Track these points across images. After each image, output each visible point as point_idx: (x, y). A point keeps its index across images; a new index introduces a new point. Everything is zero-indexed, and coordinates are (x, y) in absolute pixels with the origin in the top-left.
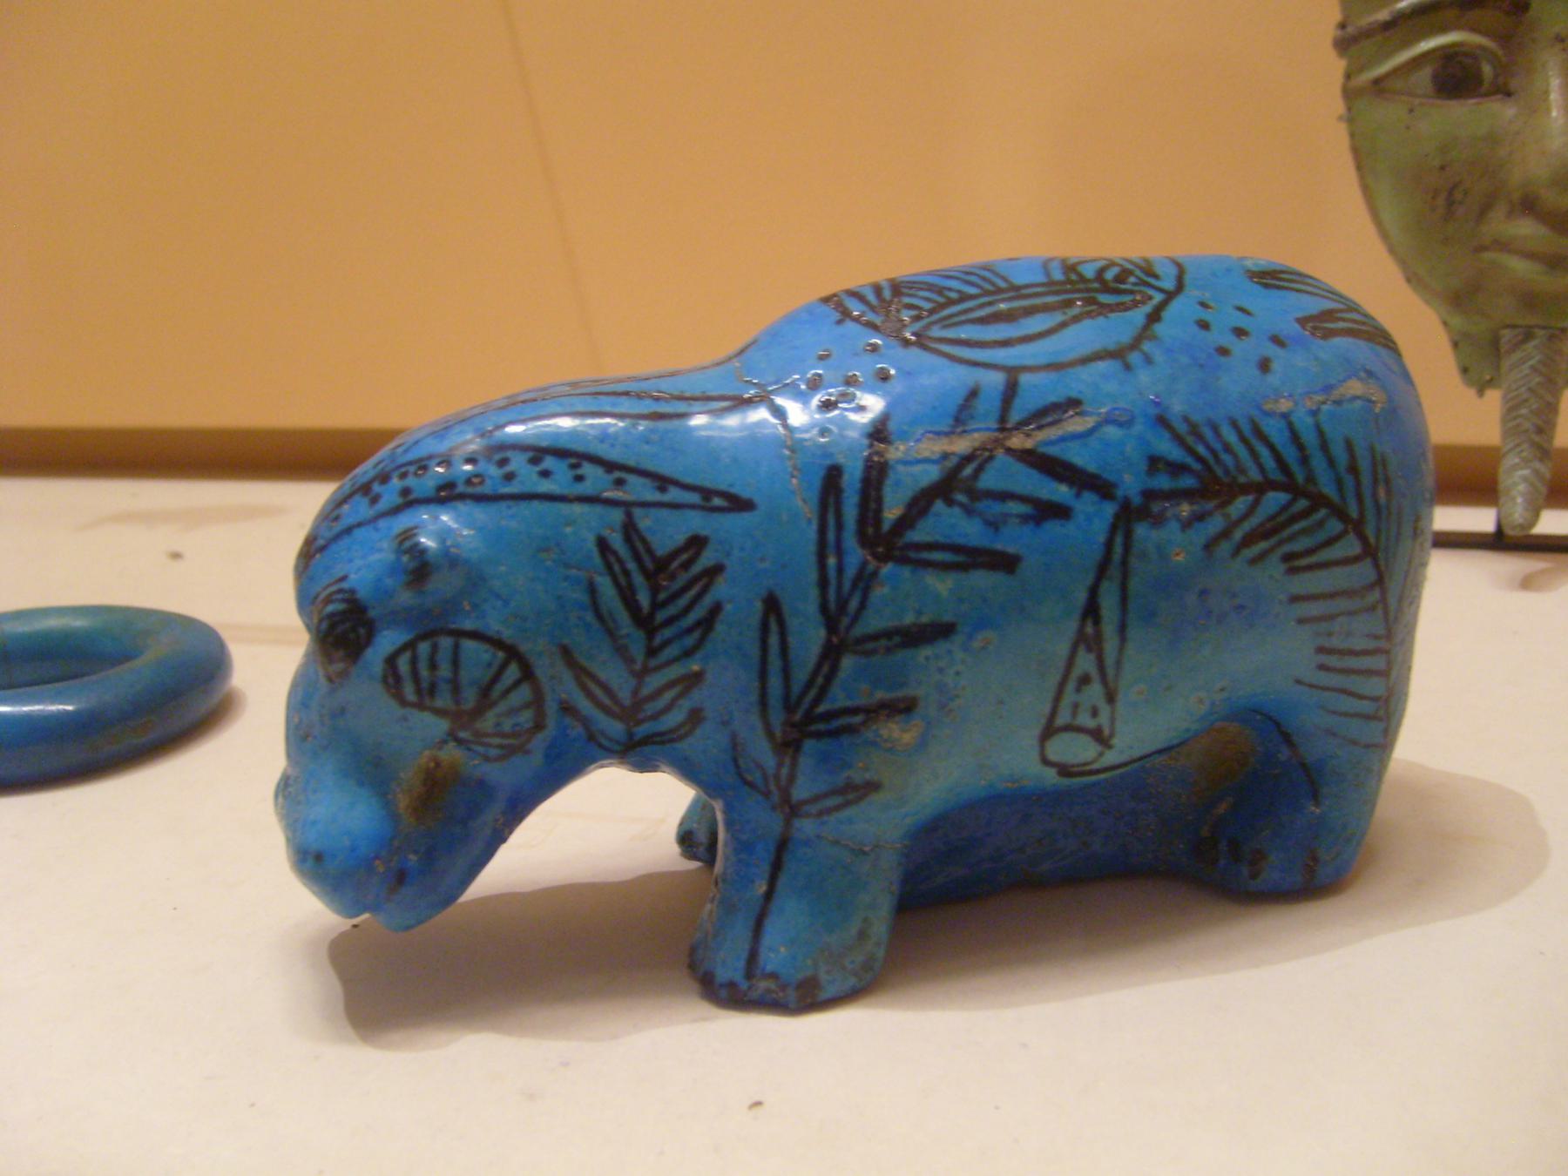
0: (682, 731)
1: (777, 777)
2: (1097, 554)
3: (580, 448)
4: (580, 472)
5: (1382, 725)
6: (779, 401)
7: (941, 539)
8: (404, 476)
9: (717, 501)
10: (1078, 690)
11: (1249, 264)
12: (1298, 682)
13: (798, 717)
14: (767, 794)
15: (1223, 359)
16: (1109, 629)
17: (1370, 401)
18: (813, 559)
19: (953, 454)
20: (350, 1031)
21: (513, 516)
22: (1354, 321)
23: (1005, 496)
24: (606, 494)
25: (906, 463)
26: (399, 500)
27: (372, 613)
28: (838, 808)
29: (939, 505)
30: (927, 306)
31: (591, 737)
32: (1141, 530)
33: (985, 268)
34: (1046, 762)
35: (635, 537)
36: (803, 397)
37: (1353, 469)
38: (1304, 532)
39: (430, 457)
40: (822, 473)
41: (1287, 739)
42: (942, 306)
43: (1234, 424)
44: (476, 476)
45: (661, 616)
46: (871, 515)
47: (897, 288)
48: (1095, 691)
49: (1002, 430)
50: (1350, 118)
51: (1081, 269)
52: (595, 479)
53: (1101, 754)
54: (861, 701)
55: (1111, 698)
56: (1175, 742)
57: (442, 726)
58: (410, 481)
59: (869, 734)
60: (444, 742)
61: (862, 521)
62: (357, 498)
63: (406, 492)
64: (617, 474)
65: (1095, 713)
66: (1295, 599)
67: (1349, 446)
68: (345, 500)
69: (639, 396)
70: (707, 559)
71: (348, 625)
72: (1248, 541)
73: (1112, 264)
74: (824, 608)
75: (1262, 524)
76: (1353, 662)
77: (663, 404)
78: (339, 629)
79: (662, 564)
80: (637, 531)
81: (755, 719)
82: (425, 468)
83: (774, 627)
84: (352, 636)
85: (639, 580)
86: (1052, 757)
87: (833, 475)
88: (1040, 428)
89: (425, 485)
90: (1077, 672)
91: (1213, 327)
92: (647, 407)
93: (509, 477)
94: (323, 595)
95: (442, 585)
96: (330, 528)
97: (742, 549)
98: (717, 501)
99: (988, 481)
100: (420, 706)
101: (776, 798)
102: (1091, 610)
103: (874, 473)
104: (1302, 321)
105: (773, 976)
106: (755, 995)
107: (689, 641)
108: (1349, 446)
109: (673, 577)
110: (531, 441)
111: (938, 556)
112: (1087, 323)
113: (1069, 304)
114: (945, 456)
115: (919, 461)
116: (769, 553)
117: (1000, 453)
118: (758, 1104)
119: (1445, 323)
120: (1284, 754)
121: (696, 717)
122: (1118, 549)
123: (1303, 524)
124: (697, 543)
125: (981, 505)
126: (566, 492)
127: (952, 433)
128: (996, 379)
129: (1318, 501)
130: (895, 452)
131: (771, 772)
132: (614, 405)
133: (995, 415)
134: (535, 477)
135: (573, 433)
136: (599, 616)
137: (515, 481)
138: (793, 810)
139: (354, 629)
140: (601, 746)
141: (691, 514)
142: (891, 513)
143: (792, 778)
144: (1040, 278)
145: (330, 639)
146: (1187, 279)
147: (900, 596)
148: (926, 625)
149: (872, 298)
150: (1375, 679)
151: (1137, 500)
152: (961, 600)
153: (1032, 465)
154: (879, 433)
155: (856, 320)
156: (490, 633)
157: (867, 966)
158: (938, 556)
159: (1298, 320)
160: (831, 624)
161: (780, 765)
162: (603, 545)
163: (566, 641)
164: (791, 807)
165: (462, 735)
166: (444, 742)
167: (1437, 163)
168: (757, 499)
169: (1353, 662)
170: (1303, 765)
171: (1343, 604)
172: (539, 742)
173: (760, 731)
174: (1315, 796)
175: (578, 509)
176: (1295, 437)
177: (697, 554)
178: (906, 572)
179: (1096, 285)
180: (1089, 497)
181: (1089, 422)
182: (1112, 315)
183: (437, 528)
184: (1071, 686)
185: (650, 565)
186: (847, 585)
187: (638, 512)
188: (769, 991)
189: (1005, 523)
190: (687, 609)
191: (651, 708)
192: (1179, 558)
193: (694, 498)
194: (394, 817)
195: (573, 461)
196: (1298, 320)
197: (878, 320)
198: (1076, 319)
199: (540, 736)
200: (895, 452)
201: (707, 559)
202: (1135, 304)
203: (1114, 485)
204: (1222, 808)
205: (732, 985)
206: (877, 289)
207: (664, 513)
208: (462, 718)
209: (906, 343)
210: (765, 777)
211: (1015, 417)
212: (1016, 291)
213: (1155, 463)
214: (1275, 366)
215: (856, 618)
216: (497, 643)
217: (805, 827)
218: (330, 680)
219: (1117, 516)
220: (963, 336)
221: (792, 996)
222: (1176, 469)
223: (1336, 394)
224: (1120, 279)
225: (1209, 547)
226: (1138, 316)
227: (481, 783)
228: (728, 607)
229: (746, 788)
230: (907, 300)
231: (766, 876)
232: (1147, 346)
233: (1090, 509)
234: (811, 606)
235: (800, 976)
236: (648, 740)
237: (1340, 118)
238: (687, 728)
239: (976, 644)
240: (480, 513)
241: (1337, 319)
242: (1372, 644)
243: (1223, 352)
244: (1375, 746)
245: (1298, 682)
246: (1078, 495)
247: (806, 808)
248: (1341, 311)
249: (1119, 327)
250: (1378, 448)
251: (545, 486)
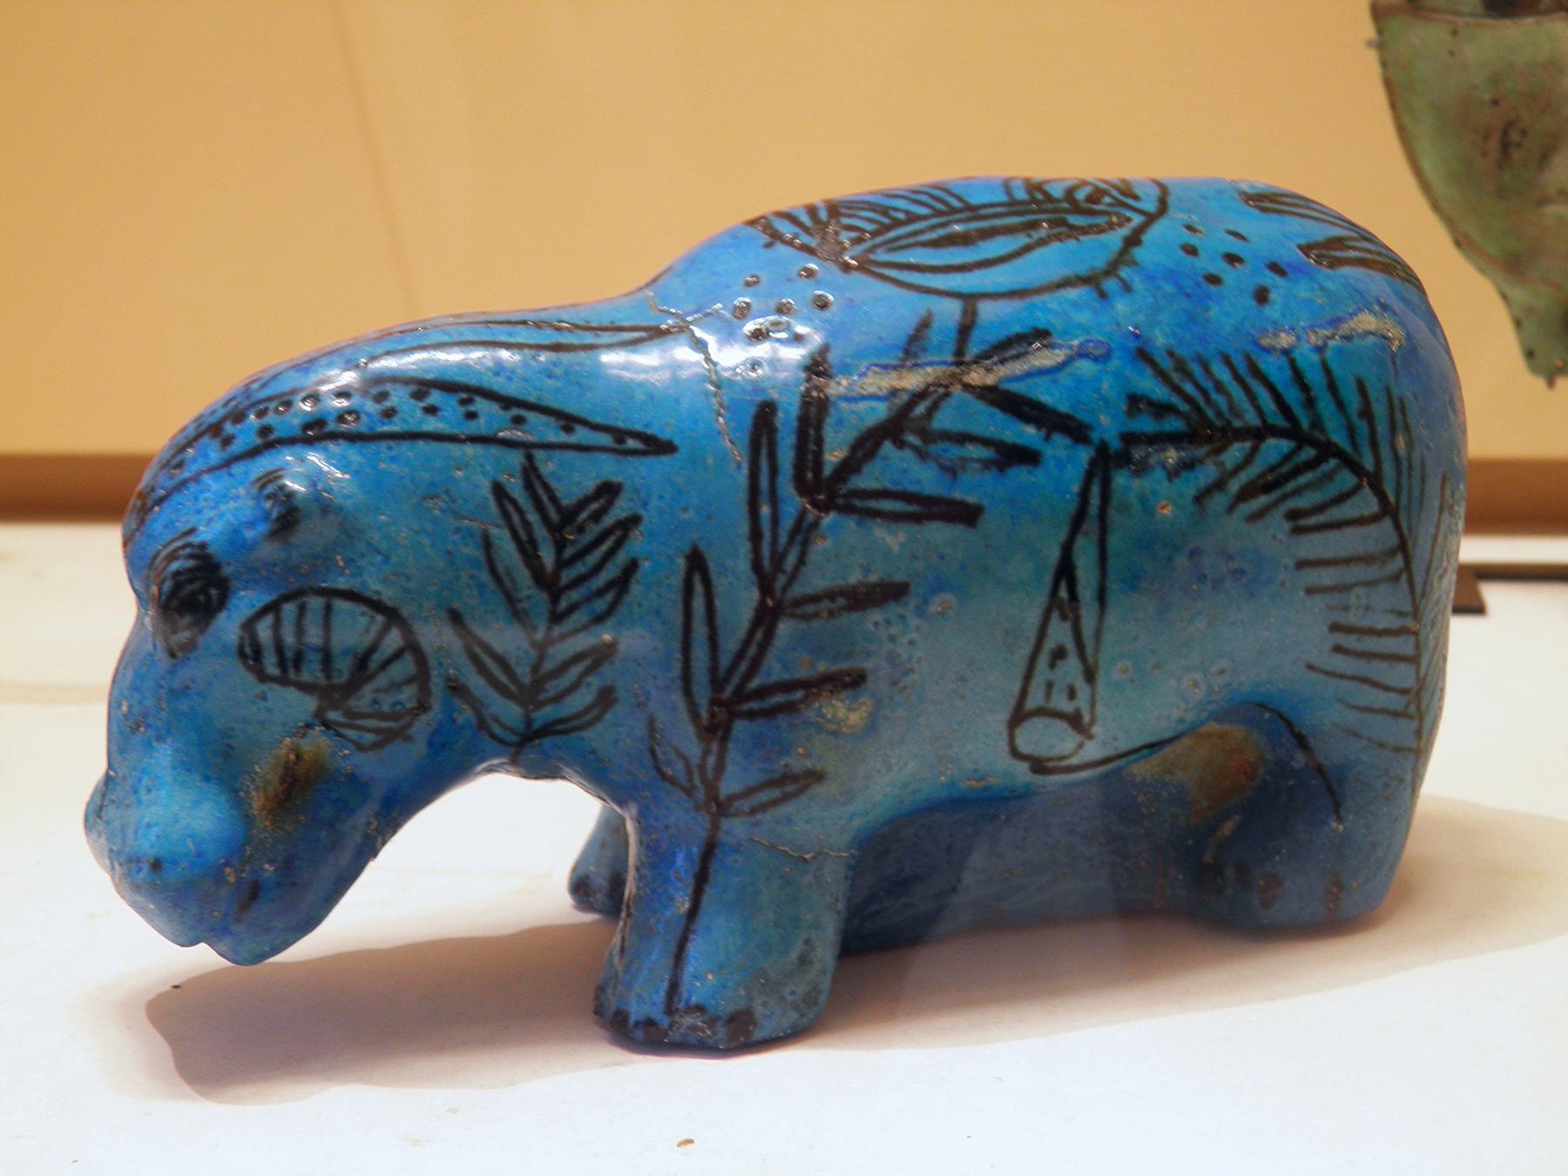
0: (588, 717)
1: (702, 768)
2: (1072, 507)
3: (473, 382)
4: (472, 408)
5: (1414, 725)
6: (698, 332)
7: (889, 485)
8: (261, 414)
9: (632, 443)
10: (1052, 666)
11: (1245, 187)
12: (1311, 667)
13: (727, 693)
14: (689, 792)
15: (1213, 289)
16: (1087, 592)
17: (1385, 337)
18: (744, 508)
19: (903, 390)
20: (186, 1088)
21: (393, 459)
22: (1369, 251)
23: (963, 438)
24: (501, 434)
25: (850, 399)
26: (259, 441)
27: (227, 571)
28: (774, 803)
29: (888, 447)
30: (870, 227)
31: (482, 724)
32: (1120, 479)
33: (936, 187)
34: (1015, 753)
35: (537, 485)
36: (728, 335)
37: (1367, 413)
38: (1308, 486)
39: (294, 392)
40: (753, 410)
41: (1301, 741)
42: (888, 228)
43: (1227, 361)
44: (350, 412)
45: (567, 576)
46: (810, 457)
47: (835, 209)
48: (1071, 668)
49: (959, 364)
50: (1381, 45)
51: (1047, 188)
52: (489, 416)
53: (1080, 746)
54: (802, 673)
55: (1090, 675)
56: (1167, 735)
57: (310, 703)
58: (270, 419)
59: (810, 713)
60: (309, 726)
61: (799, 467)
62: (206, 440)
63: (265, 431)
64: (516, 411)
65: (1072, 694)
66: (1302, 564)
67: (1362, 388)
68: (190, 443)
69: (538, 325)
70: (621, 509)
71: (196, 585)
72: (1246, 494)
73: (1084, 183)
74: (756, 566)
75: (1262, 475)
76: (1371, 644)
77: (568, 337)
78: (189, 588)
79: (569, 515)
80: (539, 477)
81: (677, 697)
82: (288, 404)
83: (698, 588)
84: (201, 598)
85: (541, 532)
86: (1023, 747)
87: (765, 413)
88: (1002, 361)
89: (287, 423)
90: (1049, 645)
91: (1201, 253)
92: (548, 337)
93: (389, 414)
94: (164, 554)
95: (310, 536)
96: (172, 477)
97: (661, 497)
98: (632, 443)
99: (944, 420)
100: (283, 681)
101: (701, 794)
102: (1065, 571)
103: (813, 410)
104: (1306, 249)
105: (700, 1009)
106: (675, 1035)
107: (601, 605)
108: (1362, 388)
109: (581, 530)
110: (419, 375)
111: (887, 505)
112: (1055, 246)
113: (1034, 225)
114: (894, 392)
115: (864, 398)
116: (694, 502)
117: (957, 390)
118: (690, 1141)
119: (1504, 297)
120: (1299, 760)
121: (606, 698)
122: (1095, 501)
123: (1308, 477)
124: (609, 491)
125: (934, 449)
126: (456, 431)
127: (903, 366)
128: (950, 311)
129: (1327, 450)
130: (837, 387)
131: (695, 761)
132: (510, 334)
133: (951, 346)
134: (419, 413)
135: (462, 366)
136: (493, 571)
137: (395, 419)
138: (721, 808)
139: (204, 590)
140: (493, 736)
141: (603, 457)
142: (833, 456)
143: (720, 767)
144: (1001, 197)
145: (175, 603)
146: (1171, 200)
147: (844, 551)
148: (876, 585)
149: (805, 219)
150: (1403, 666)
151: (1115, 444)
152: (915, 557)
153: (993, 403)
154: (816, 367)
155: (790, 243)
156: (367, 594)
157: (810, 999)
158: (887, 505)
159: (1301, 248)
160: (766, 587)
161: (706, 752)
162: (499, 491)
163: (456, 605)
164: (719, 805)
165: (333, 716)
166: (309, 726)
167: (1487, 97)
168: (677, 441)
169: (1371, 644)
170: (1320, 770)
171: (1358, 572)
172: (422, 726)
173: (683, 714)
174: (1337, 807)
175: (470, 450)
176: (1298, 375)
177: (610, 504)
178: (850, 523)
179: (1066, 205)
180: (1060, 440)
181: (1059, 356)
182: (1083, 238)
183: (308, 470)
184: (1043, 659)
185: (553, 514)
186: (783, 538)
187: (539, 455)
188: (694, 1028)
189: (964, 468)
190: (597, 569)
191: (552, 688)
192: (1165, 511)
193: (605, 439)
194: (248, 819)
195: (464, 396)
196: (1301, 248)
197: (813, 242)
198: (1042, 242)
199: (424, 718)
200: (837, 387)
201: (621, 509)
202: (1111, 226)
203: (1088, 427)
204: (1228, 828)
205: (650, 1023)
206: (812, 211)
207: (570, 455)
208: (333, 694)
209: (846, 268)
210: (689, 771)
211: (973, 350)
212: (973, 212)
213: (1135, 402)
214: (1274, 296)
215: (794, 576)
216: (376, 606)
217: (735, 828)
218: (172, 655)
219: (1093, 462)
220: (912, 260)
221: (722, 1031)
222: (1161, 410)
223: (1344, 328)
224: (1092, 199)
225: (1200, 498)
226: (1115, 239)
227: (352, 778)
228: (646, 565)
229: (667, 785)
230: (845, 221)
231: (690, 891)
232: (1124, 272)
233: (1062, 454)
234: (743, 564)
235: (731, 1008)
236: (548, 730)
237: (1370, 44)
238: (595, 713)
239: (933, 608)
240: (353, 453)
241: (1343, 247)
242: (1394, 623)
243: (1214, 280)
244: (1409, 750)
245: (1311, 667)
246: (1047, 438)
247: (737, 804)
248: (1350, 239)
249: (1096, 250)
250: (1395, 391)
251: (431, 424)
